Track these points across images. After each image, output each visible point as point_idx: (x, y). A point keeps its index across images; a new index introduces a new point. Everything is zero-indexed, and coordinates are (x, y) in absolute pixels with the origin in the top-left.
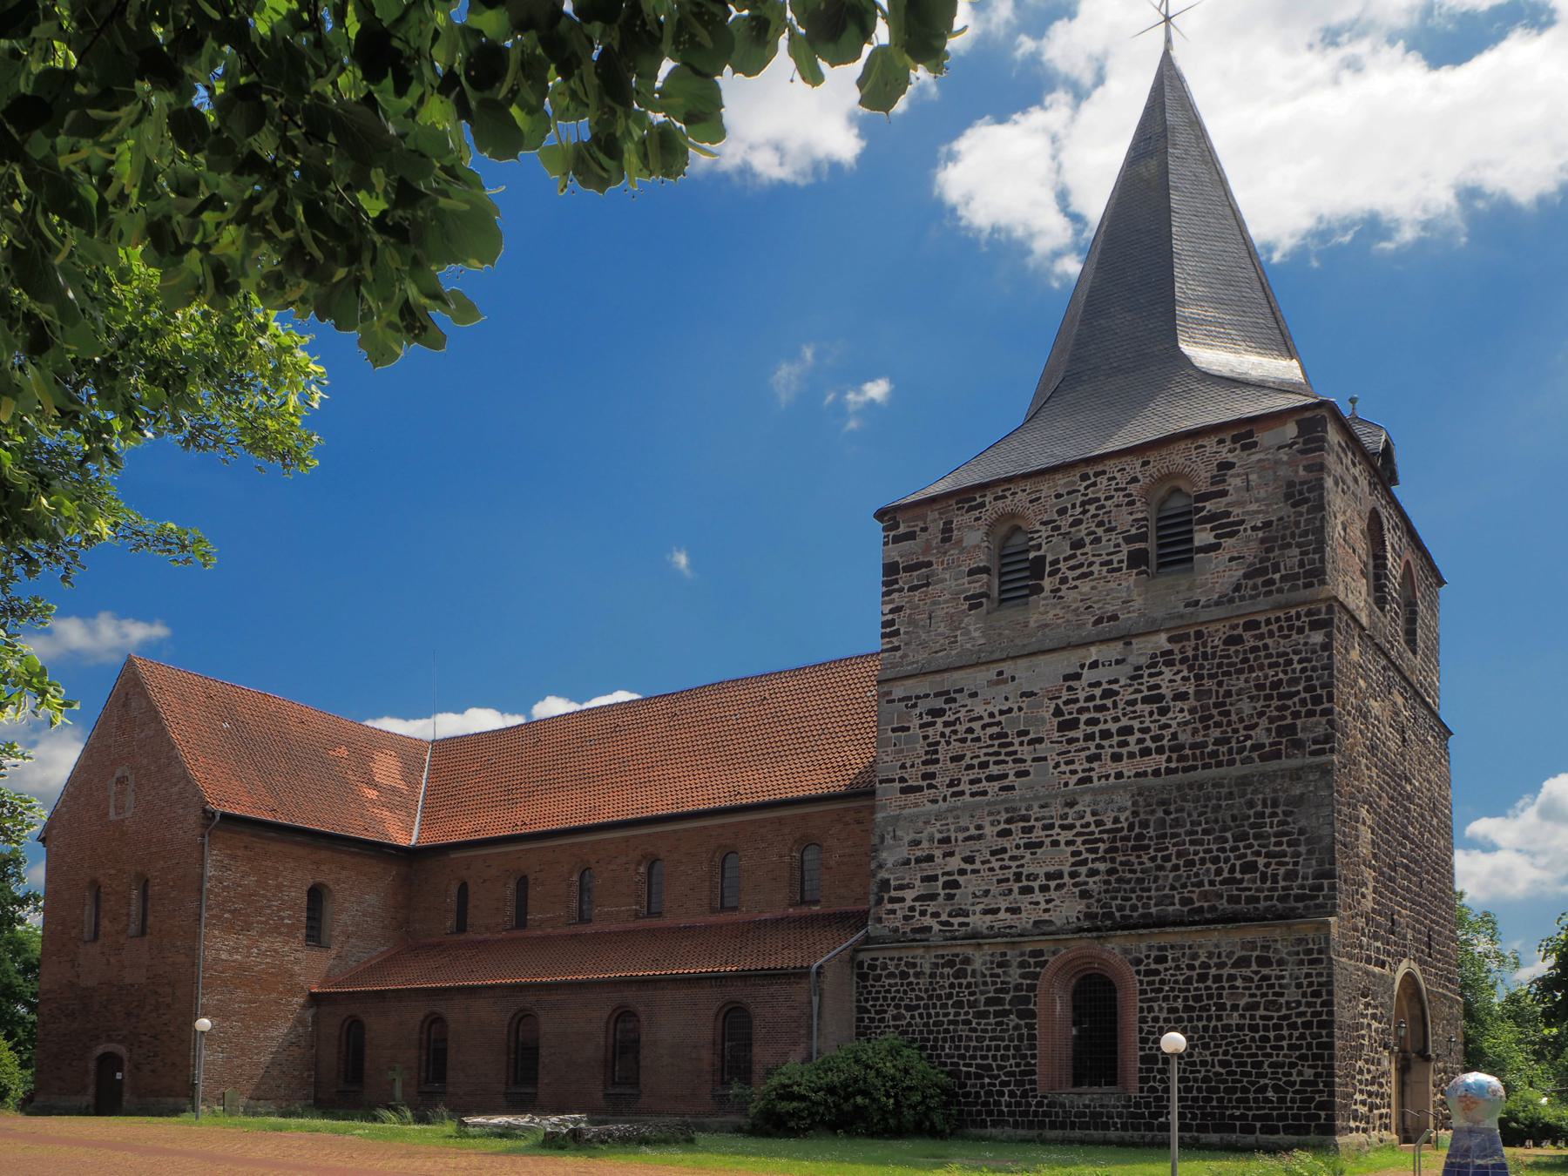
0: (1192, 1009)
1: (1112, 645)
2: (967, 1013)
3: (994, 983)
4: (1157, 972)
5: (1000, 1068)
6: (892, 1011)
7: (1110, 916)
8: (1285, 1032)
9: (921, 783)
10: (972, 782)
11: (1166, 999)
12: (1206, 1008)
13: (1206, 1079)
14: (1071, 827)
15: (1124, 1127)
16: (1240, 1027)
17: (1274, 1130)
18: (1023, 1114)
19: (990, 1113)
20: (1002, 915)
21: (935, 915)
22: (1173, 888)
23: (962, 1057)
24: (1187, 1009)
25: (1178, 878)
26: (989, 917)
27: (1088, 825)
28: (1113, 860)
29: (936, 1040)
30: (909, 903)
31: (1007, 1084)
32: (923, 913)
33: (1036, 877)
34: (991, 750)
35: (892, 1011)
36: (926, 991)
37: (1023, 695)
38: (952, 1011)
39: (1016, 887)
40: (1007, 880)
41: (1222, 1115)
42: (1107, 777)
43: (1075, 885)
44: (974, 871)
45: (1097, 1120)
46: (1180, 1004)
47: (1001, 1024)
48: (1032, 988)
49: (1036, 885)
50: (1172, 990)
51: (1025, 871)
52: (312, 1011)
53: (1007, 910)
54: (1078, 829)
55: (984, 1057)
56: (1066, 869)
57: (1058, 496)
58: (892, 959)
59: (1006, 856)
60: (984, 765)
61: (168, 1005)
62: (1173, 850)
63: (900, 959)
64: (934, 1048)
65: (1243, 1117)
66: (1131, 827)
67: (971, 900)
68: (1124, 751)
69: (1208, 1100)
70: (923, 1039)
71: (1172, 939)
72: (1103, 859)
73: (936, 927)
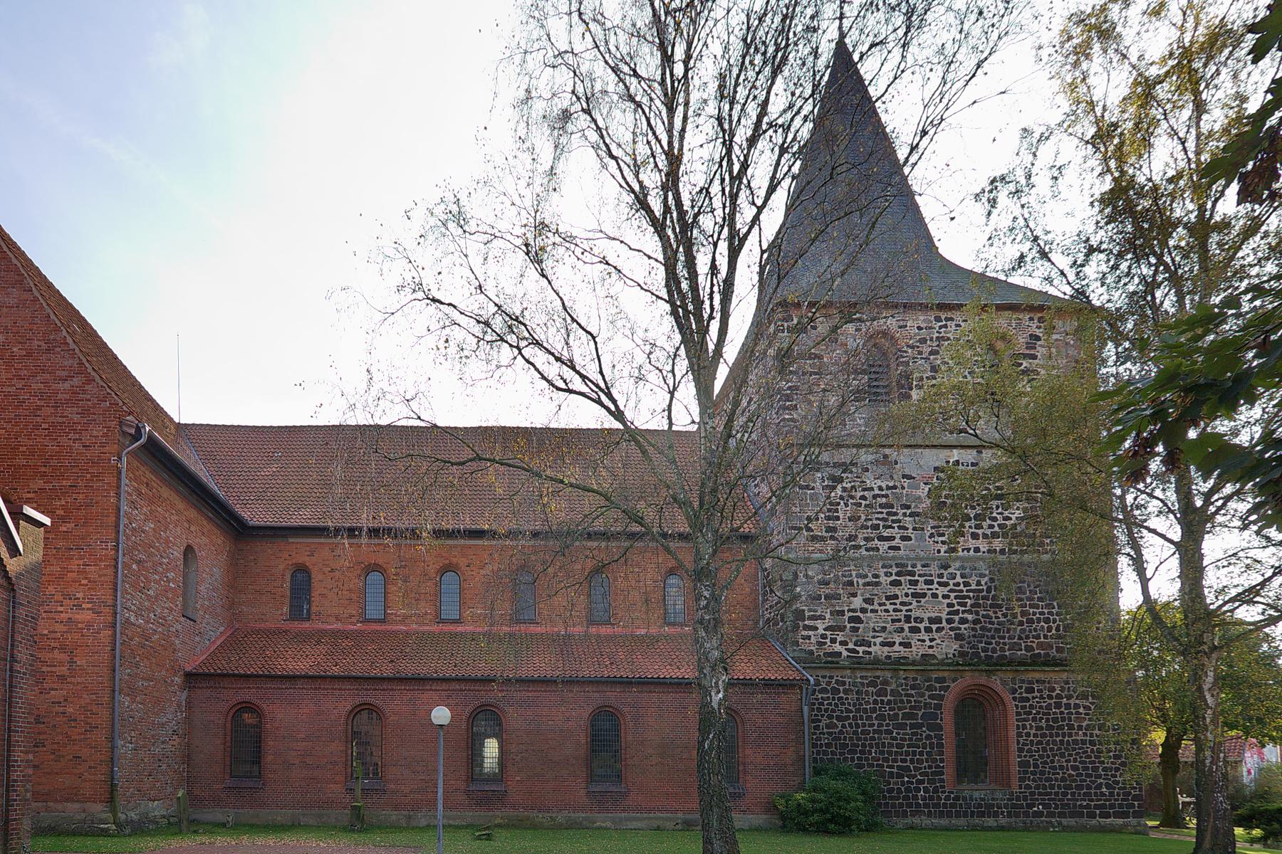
0: (1052, 728)
1: (969, 451)
2: (888, 725)
3: (909, 702)
4: (1027, 700)
5: (916, 769)
6: (825, 721)
7: (977, 655)
8: (1112, 746)
9: (824, 534)
10: (866, 539)
11: (1034, 719)
12: (1061, 727)
13: (1063, 779)
14: (946, 584)
15: (1009, 815)
16: (1084, 742)
17: (1107, 816)
18: (935, 806)
19: (909, 805)
20: (897, 648)
21: (843, 643)
22: (1020, 638)
23: (886, 760)
24: (1049, 727)
25: (1023, 631)
26: (886, 649)
27: (958, 584)
28: (977, 613)
29: (864, 745)
30: (821, 631)
31: (922, 782)
32: (833, 641)
33: (922, 620)
34: (880, 516)
35: (825, 721)
36: (854, 705)
37: (904, 476)
38: (876, 722)
39: (906, 626)
40: (899, 620)
41: (1075, 805)
42: (968, 550)
43: (951, 629)
44: (872, 611)
45: (987, 810)
46: (1043, 723)
47: (916, 734)
48: (939, 707)
49: (922, 626)
50: (1038, 713)
51: (913, 614)
52: (184, 695)
53: (901, 644)
54: (951, 587)
55: (904, 761)
56: (944, 616)
57: (920, 328)
58: (824, 677)
59: (897, 602)
60: (876, 527)
61: (62, 678)
62: (1018, 610)
63: (831, 677)
64: (862, 752)
65: (1088, 806)
66: (989, 590)
67: (872, 634)
68: (980, 532)
69: (1065, 794)
70: (853, 745)
71: (1037, 676)
72: (970, 612)
73: (845, 653)
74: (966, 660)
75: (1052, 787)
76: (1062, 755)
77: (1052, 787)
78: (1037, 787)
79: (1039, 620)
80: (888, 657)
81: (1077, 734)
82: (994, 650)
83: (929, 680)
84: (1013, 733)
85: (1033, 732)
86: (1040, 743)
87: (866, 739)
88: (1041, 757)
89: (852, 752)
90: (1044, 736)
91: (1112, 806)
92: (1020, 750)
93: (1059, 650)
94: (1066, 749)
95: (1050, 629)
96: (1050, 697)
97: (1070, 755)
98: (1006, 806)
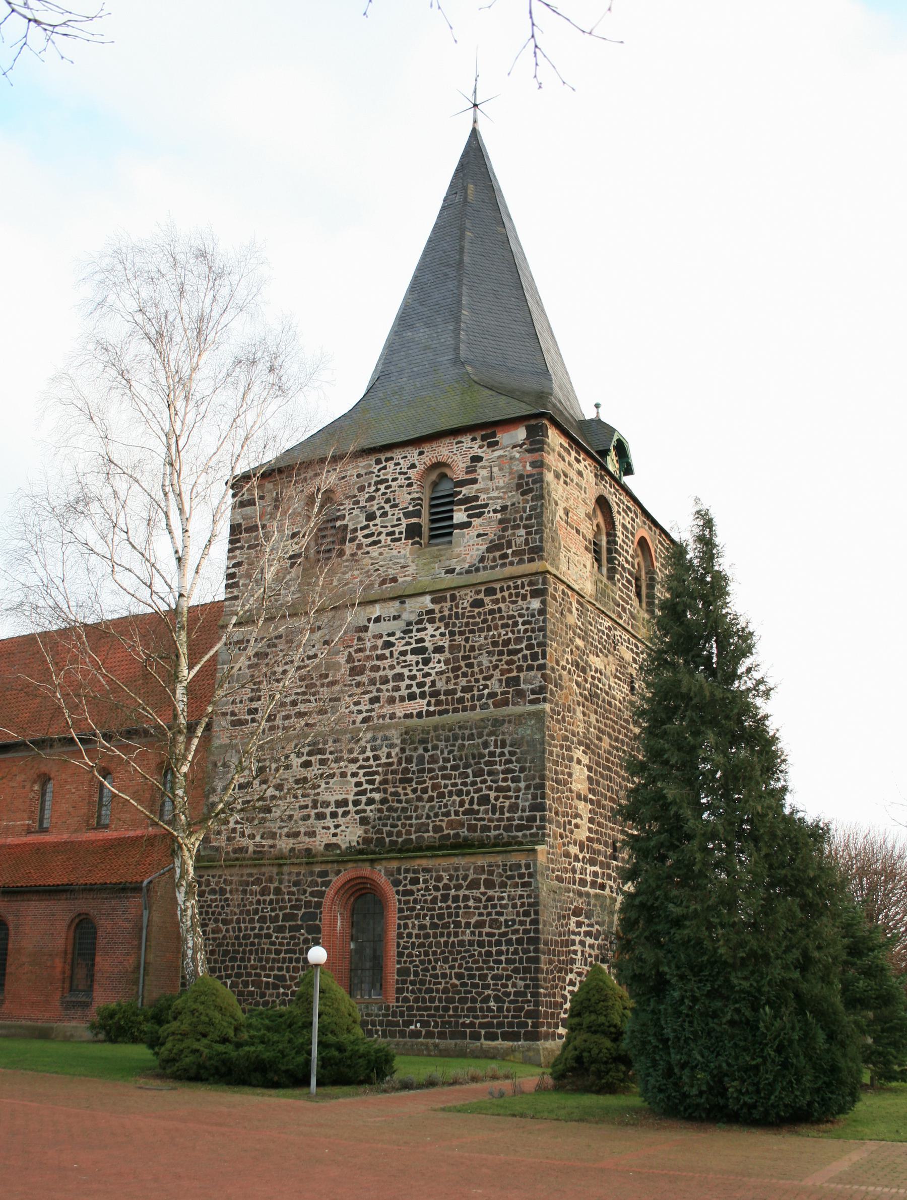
1: (391, 603)
4: (411, 893)
7: (380, 841)
13: (446, 990)
15: (384, 1035)
16: (471, 943)
17: (492, 1037)
20: (302, 838)
23: (263, 968)
24: (434, 926)
25: (432, 808)
26: (292, 841)
29: (244, 952)
38: (257, 925)
40: (306, 807)
41: (457, 1023)
43: (357, 812)
46: (427, 921)
48: (319, 905)
49: (328, 811)
50: (422, 908)
53: (305, 834)
54: (361, 763)
55: (280, 969)
57: (359, 476)
62: (429, 783)
63: (220, 877)
64: (242, 960)
65: (472, 1025)
69: (446, 1009)
70: (235, 951)
72: (377, 790)
74: (369, 851)
75: (432, 1000)
76: (446, 960)
77: (432, 1000)
78: (416, 1000)
79: (451, 794)
80: (292, 850)
81: (464, 933)
82: (399, 834)
83: (312, 873)
84: (393, 934)
85: (416, 931)
86: (422, 945)
87: (246, 945)
88: (422, 962)
89: (233, 959)
90: (427, 936)
91: (500, 1025)
92: (400, 955)
93: (472, 828)
94: (450, 952)
95: (462, 804)
96: (436, 888)
97: (455, 960)
98: (381, 1023)
